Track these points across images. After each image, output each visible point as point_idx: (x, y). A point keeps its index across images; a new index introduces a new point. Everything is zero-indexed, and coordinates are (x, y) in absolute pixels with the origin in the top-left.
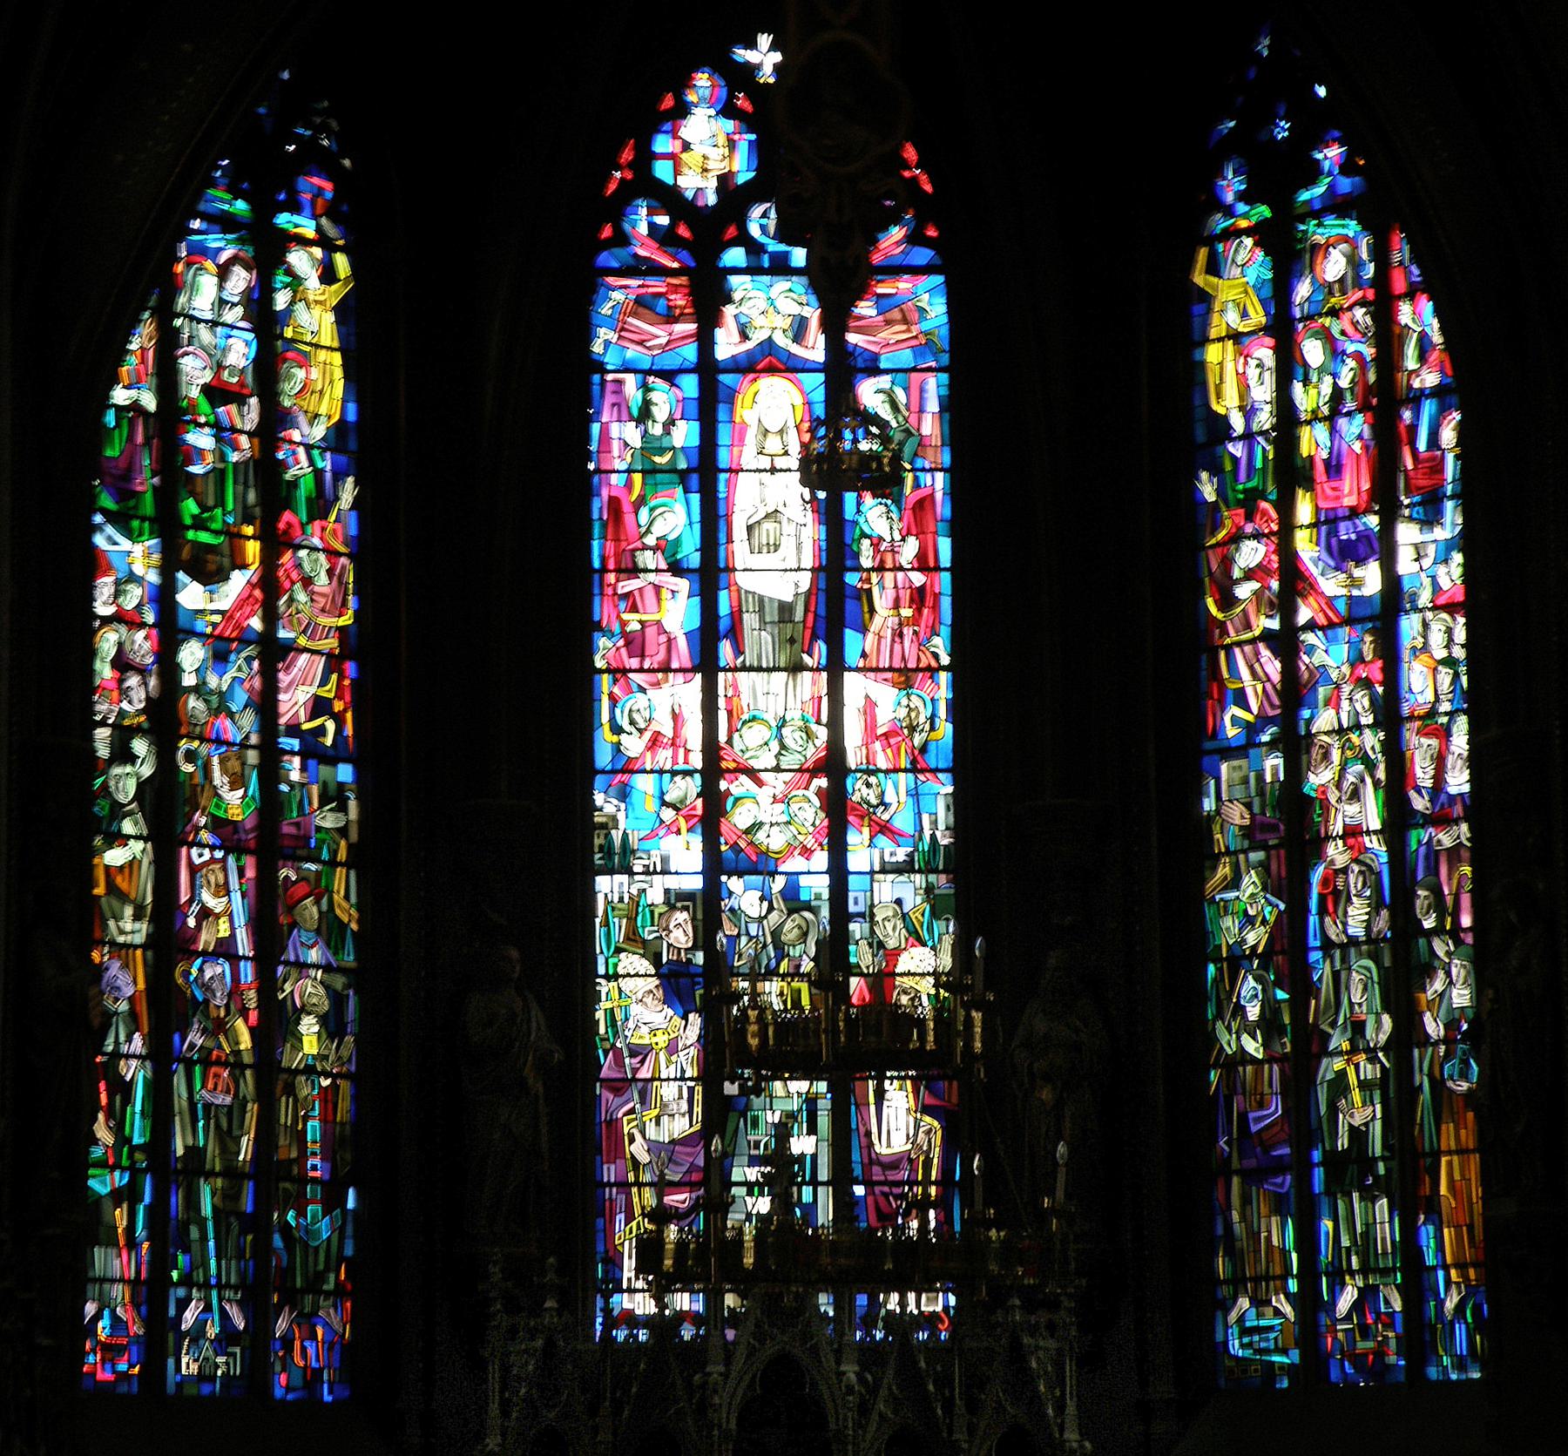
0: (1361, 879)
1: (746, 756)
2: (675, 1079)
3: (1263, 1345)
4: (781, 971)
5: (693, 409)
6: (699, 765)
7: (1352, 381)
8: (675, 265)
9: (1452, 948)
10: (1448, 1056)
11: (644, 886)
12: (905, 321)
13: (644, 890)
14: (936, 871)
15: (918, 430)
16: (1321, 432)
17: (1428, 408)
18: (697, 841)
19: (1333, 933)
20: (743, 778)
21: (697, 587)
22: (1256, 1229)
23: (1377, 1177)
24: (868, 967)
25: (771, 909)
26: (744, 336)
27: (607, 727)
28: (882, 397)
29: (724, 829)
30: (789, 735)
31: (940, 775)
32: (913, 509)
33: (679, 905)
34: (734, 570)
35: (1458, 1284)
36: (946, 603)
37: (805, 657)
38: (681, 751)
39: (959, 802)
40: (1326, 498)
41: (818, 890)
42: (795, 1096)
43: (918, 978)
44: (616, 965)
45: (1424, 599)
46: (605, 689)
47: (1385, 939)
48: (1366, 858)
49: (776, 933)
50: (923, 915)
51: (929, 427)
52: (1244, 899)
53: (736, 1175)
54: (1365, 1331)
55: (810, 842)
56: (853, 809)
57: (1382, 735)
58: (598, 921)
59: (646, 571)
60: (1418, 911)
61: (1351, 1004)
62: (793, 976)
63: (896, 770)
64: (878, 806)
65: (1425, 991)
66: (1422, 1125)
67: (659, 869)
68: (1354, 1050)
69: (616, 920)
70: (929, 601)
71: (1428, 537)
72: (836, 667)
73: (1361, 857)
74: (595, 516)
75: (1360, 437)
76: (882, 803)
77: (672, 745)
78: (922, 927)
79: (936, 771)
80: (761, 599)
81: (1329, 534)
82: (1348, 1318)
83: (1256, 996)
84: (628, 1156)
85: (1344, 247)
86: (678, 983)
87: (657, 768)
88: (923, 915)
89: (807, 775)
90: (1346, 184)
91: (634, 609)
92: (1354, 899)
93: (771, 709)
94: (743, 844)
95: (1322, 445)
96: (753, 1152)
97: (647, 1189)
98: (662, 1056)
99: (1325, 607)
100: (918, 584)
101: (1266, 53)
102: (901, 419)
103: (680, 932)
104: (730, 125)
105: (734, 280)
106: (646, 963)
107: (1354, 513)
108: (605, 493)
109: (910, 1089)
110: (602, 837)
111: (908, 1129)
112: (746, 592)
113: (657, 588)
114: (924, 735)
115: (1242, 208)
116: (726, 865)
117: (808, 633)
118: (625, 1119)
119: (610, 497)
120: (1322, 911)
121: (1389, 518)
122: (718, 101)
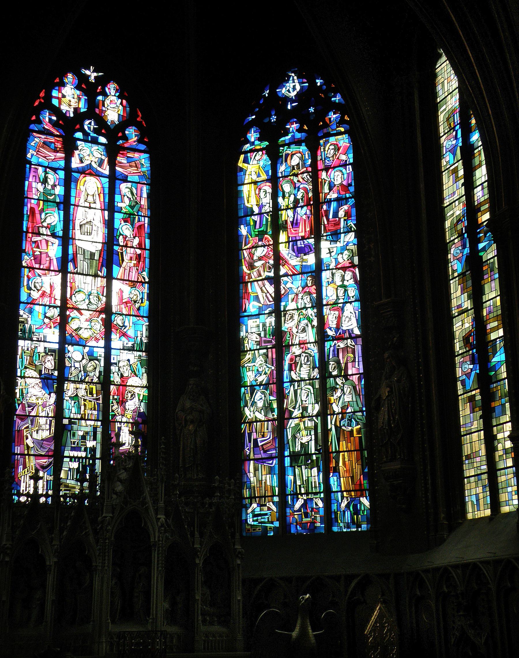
0: (306, 358)
1: (76, 304)
2: (45, 417)
3: (262, 520)
4: (86, 381)
5: (62, 182)
6: (59, 305)
7: (302, 196)
8: (58, 134)
9: (344, 381)
10: (342, 418)
11: (37, 345)
12: (136, 166)
13: (37, 347)
14: (142, 351)
15: (140, 203)
16: (290, 213)
17: (334, 205)
18: (57, 331)
19: (294, 376)
20: (75, 311)
21: (61, 243)
22: (260, 479)
23: (312, 461)
24: (117, 382)
25: (83, 358)
26: (81, 161)
27: (26, 287)
28: (128, 190)
29: (67, 328)
30: (92, 298)
31: (144, 318)
32: (137, 228)
33: (49, 353)
34: (75, 239)
35: (347, 497)
36: (147, 260)
37: (99, 272)
38: (53, 299)
39: (150, 328)
40: (292, 233)
41: (100, 354)
42: (89, 426)
43: (135, 388)
44: (24, 373)
45: (333, 266)
46: (26, 274)
47: (316, 379)
48: (308, 351)
49: (84, 367)
50: (137, 366)
51: (144, 202)
52: (257, 366)
53: (66, 453)
54: (306, 515)
55: (98, 336)
56: (114, 327)
57: (315, 310)
58: (18, 356)
59: (43, 235)
60: (330, 369)
61: (302, 401)
62: (90, 383)
63: (129, 315)
64: (123, 326)
65: (333, 396)
66: (331, 442)
67: (42, 340)
68: (303, 417)
69: (26, 357)
70: (142, 259)
71: (333, 245)
72: (109, 277)
73: (306, 351)
74: (25, 213)
75: (306, 214)
76: (124, 326)
77: (49, 296)
78: (136, 370)
79: (143, 317)
80: (84, 250)
81: (293, 246)
82: (299, 510)
83: (261, 398)
84: (25, 444)
85: (299, 155)
86: (47, 382)
87: (44, 304)
88: (137, 366)
89: (98, 313)
90: (298, 135)
91: (38, 247)
92: (303, 365)
93: (87, 289)
94: (74, 334)
95: (290, 216)
96: (73, 446)
97: (32, 457)
98: (40, 408)
99: (291, 268)
100: (138, 253)
101: (267, 95)
102: (134, 198)
103: (50, 363)
104: (78, 92)
105: (79, 143)
106: (36, 373)
107: (303, 238)
108: (29, 205)
109: (130, 427)
110: (22, 326)
111: (129, 441)
112: (79, 247)
113: (47, 241)
114: (139, 304)
115: (257, 142)
116: (68, 341)
117: (100, 264)
118: (25, 430)
119: (31, 207)
120: (290, 369)
121: (318, 239)
122: (75, 84)
